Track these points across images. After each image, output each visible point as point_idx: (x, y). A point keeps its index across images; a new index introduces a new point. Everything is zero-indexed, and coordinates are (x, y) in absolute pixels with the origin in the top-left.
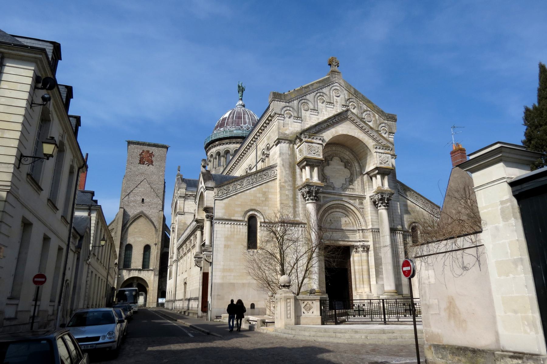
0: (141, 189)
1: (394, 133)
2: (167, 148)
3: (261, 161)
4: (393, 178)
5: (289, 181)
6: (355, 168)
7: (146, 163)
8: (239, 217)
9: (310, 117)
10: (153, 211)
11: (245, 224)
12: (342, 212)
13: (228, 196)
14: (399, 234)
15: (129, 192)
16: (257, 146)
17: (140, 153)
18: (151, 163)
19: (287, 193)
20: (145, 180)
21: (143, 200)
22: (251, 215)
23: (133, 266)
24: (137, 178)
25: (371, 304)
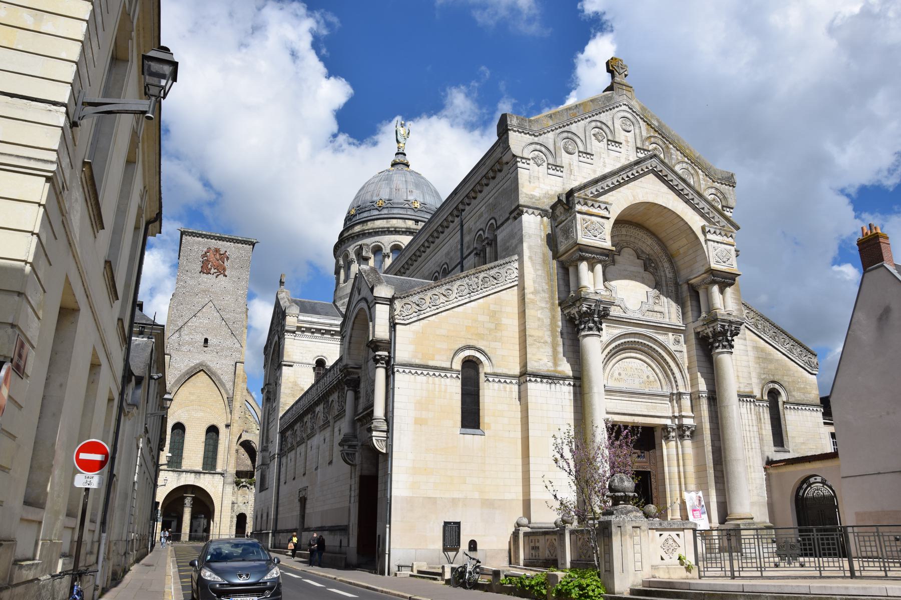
0: (201, 321)
1: (732, 208)
2: (253, 244)
3: (473, 253)
4: (733, 293)
5: (543, 291)
6: (664, 271)
7: (213, 271)
8: (442, 361)
9: (579, 166)
10: (224, 362)
11: (457, 377)
12: (640, 359)
13: (421, 317)
14: (748, 403)
15: (180, 325)
16: (462, 226)
17: (204, 253)
18: (221, 271)
19: (539, 316)
20: (211, 304)
21: (206, 340)
22: (467, 359)
23: (186, 465)
24: (196, 300)
25: (758, 538)
